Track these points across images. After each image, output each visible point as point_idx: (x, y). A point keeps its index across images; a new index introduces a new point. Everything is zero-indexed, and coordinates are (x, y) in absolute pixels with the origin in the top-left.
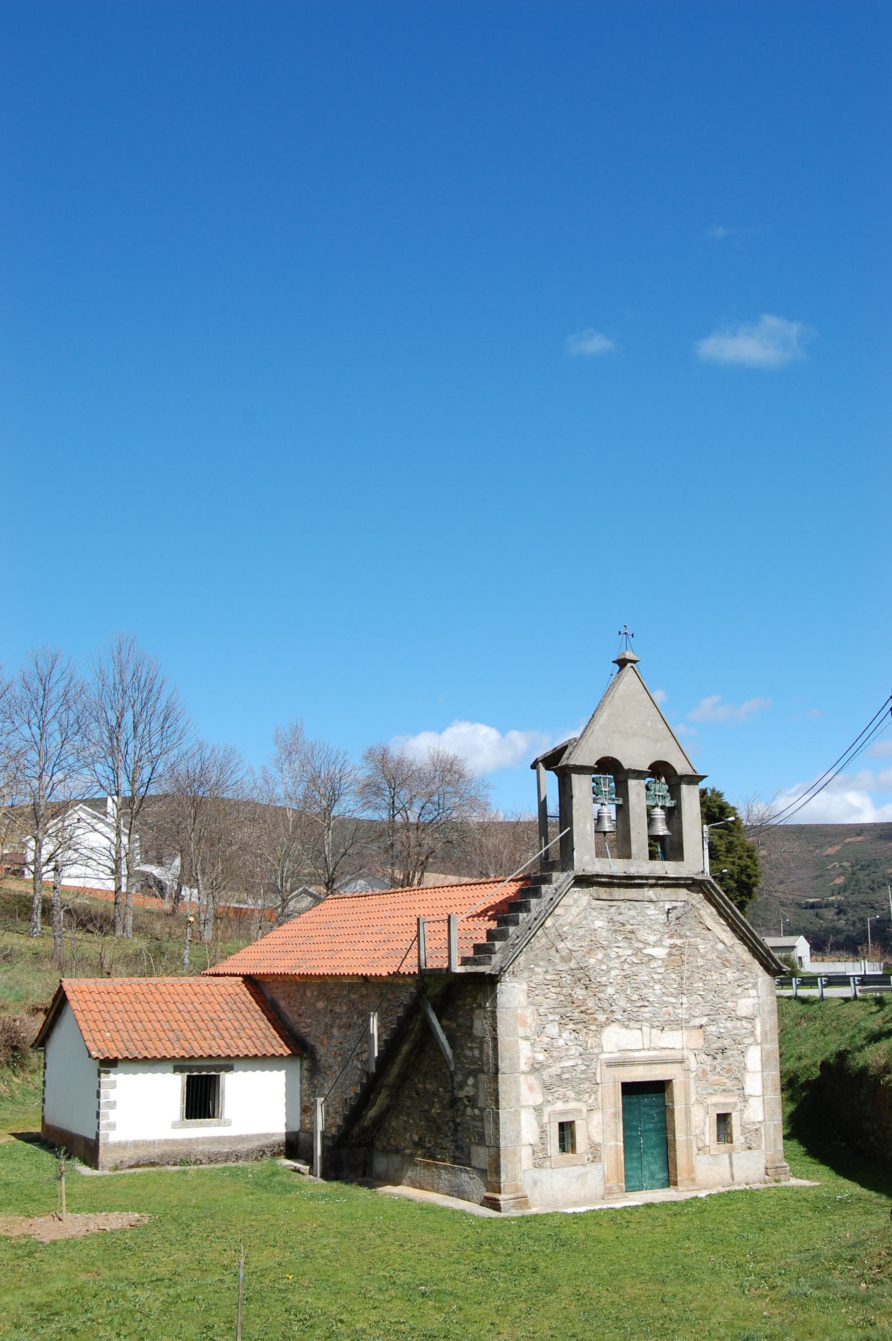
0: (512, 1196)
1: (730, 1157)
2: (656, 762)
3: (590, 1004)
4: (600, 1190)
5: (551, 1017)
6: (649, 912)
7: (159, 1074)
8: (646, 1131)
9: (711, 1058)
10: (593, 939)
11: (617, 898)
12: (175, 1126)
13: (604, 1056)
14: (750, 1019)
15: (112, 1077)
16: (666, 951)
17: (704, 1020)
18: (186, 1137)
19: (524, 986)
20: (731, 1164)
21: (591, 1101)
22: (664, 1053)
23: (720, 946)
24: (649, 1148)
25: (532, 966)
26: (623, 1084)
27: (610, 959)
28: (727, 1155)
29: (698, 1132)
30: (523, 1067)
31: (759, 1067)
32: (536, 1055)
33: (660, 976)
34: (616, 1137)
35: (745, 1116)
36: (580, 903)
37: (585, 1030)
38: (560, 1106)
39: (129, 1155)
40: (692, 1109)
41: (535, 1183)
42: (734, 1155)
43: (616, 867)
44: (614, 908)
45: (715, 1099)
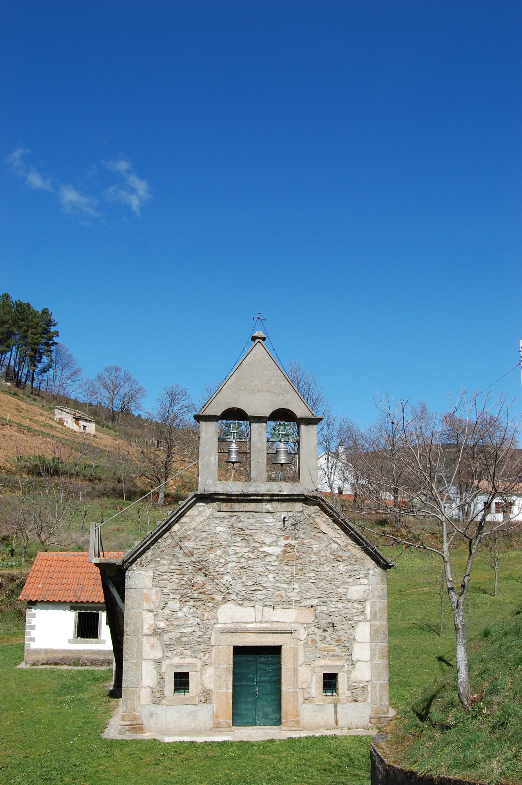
0: (129, 723)
1: (335, 706)
2: (288, 410)
3: (209, 587)
4: (210, 724)
5: (172, 596)
6: (267, 520)
7: (61, 611)
8: (261, 682)
9: (321, 630)
10: (214, 540)
11: (237, 510)
12: (70, 642)
13: (219, 626)
14: (362, 602)
15: (33, 611)
16: (282, 549)
17: (315, 602)
18: (76, 649)
19: (150, 573)
20: (336, 712)
21: (206, 658)
22: (275, 625)
23: (335, 546)
24: (263, 695)
25: (159, 559)
26: (234, 647)
27: (228, 555)
28: (333, 705)
29: (304, 686)
30: (146, 631)
31: (368, 638)
32: (158, 623)
33: (275, 568)
34: (227, 685)
35: (352, 676)
36: (204, 514)
37: (204, 606)
38: (177, 660)
39: (42, 657)
40: (300, 668)
41: (151, 715)
42: (339, 706)
43: (235, 487)
44: (235, 518)
45: (322, 662)
